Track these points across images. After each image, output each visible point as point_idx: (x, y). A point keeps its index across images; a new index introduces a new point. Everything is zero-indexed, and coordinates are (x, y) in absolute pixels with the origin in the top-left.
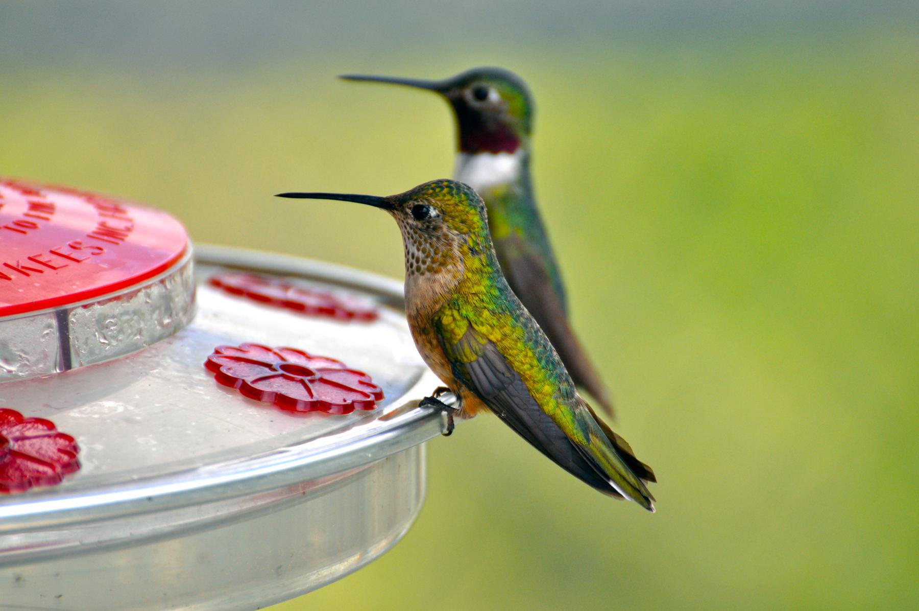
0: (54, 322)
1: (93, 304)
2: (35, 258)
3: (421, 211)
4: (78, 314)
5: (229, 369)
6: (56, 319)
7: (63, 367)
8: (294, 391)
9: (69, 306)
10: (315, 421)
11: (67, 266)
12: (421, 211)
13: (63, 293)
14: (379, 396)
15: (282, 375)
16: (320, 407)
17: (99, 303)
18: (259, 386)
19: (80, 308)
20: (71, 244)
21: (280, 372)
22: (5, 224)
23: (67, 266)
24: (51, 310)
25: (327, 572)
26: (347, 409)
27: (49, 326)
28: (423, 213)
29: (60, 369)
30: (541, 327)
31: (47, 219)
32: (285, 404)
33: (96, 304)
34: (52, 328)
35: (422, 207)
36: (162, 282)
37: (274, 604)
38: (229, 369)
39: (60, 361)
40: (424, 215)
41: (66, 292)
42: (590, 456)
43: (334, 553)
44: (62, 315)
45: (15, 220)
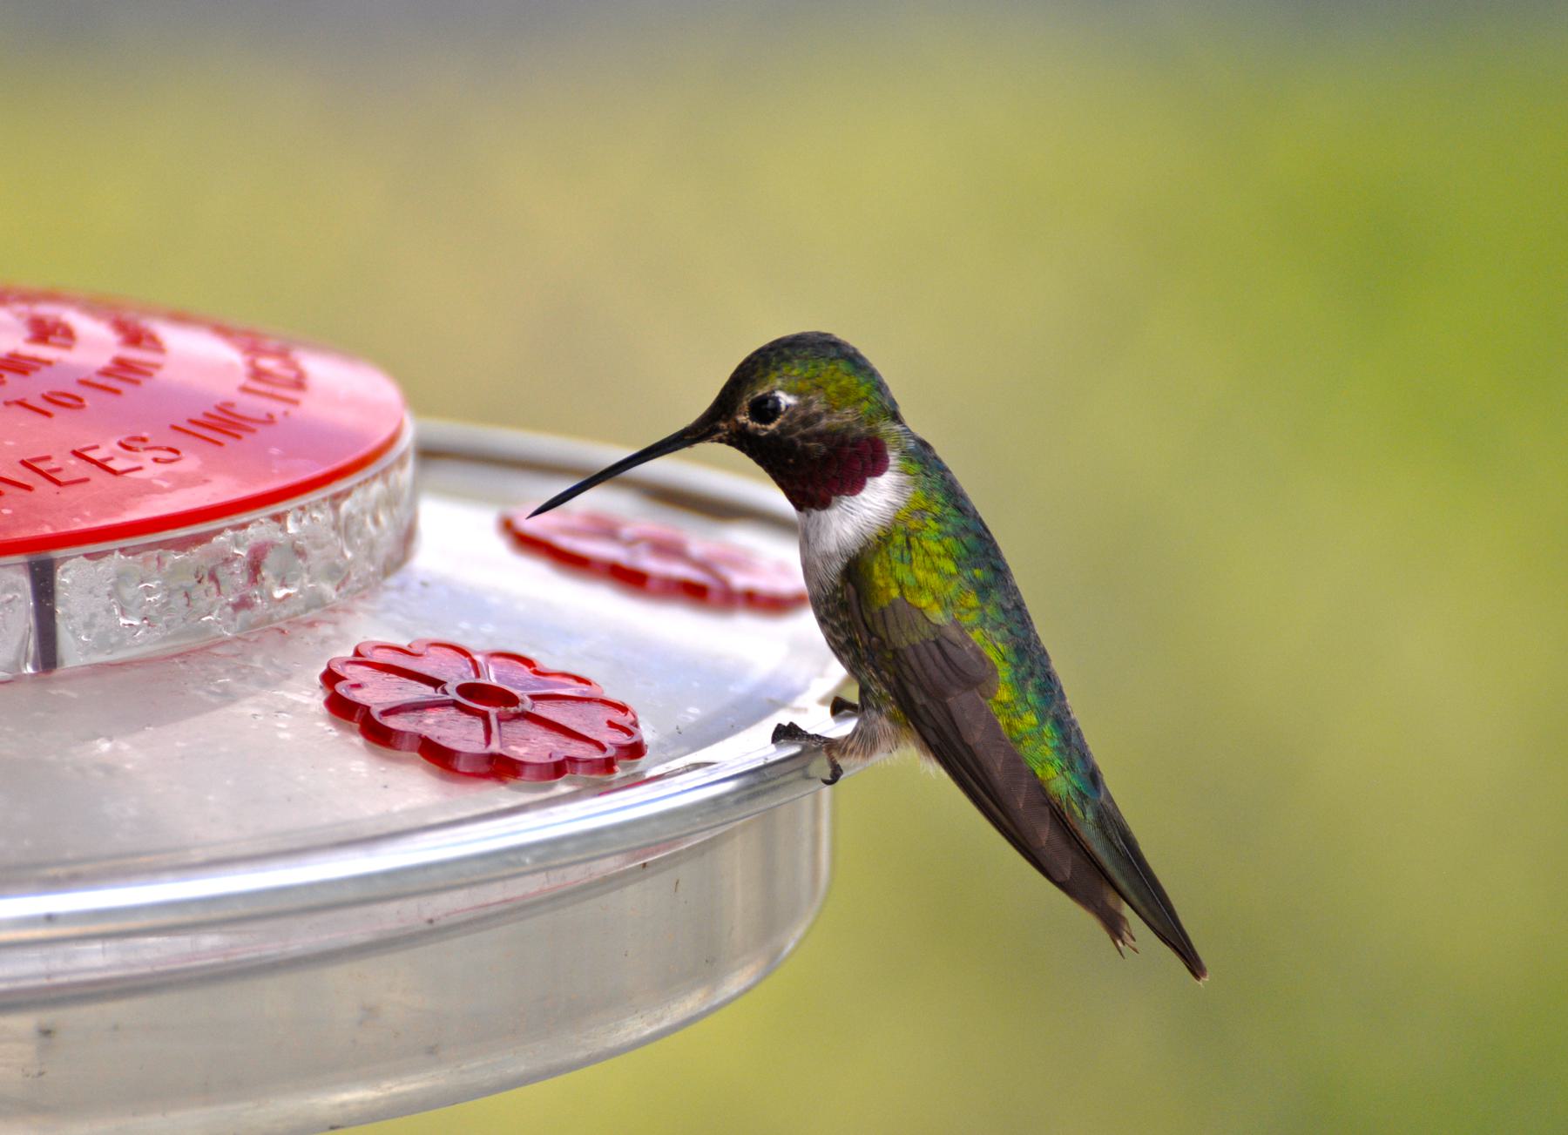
0: (25, 582)
1: (111, 552)
2: (103, 463)
3: (763, 407)
4: (72, 572)
5: (358, 686)
6: (28, 577)
7: (40, 665)
8: (462, 734)
9: (58, 554)
10: (501, 795)
11: (86, 480)
12: (763, 407)
13: (47, 530)
14: (636, 751)
15: (456, 704)
16: (501, 768)
17: (122, 550)
18: (393, 722)
19: (82, 557)
20: (123, 442)
21: (453, 695)
22: (18, 397)
23: (86, 480)
24: (21, 559)
25: (637, 1027)
26: (558, 769)
27: (14, 587)
28: (767, 409)
29: (35, 667)
30: (506, 706)
31: (295, 402)
32: (438, 756)
33: (117, 554)
34: (18, 590)
35: (763, 400)
36: (278, 518)
37: (521, 1086)
38: (358, 686)
39: (35, 653)
40: (771, 415)
41: (54, 528)
42: (1091, 852)
43: (670, 984)
44: (37, 569)
45: (218, 402)
